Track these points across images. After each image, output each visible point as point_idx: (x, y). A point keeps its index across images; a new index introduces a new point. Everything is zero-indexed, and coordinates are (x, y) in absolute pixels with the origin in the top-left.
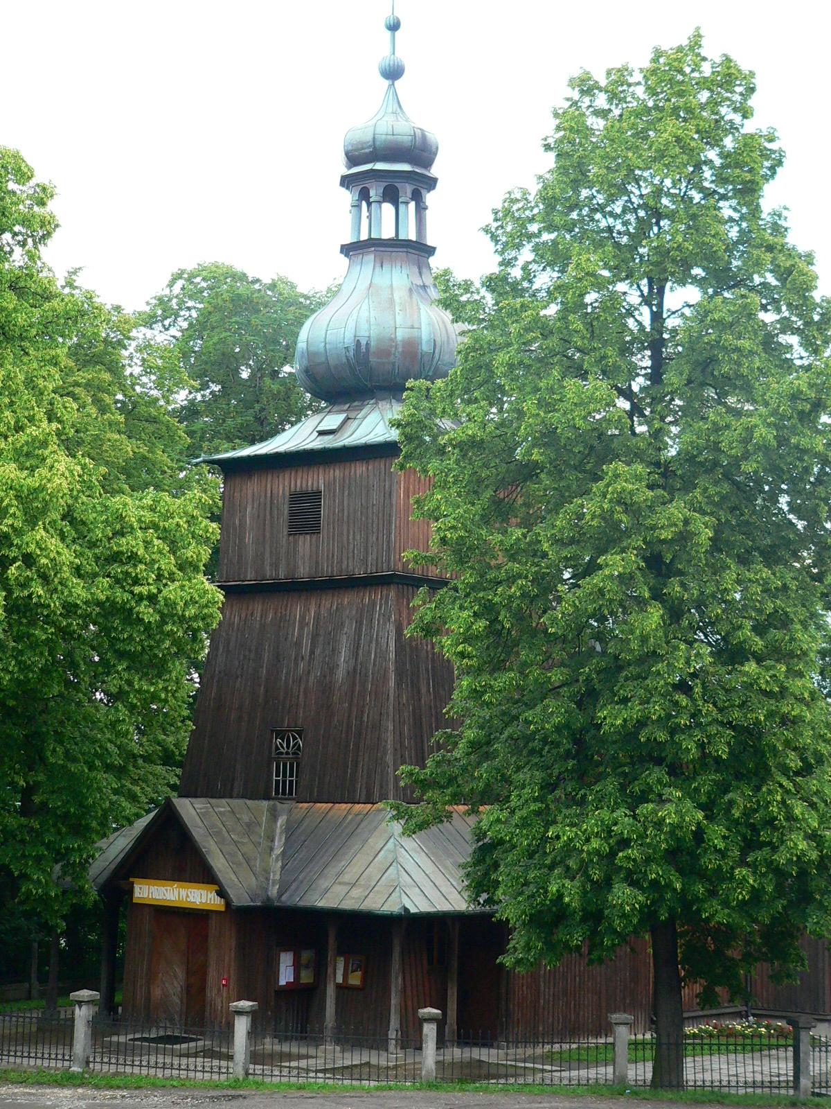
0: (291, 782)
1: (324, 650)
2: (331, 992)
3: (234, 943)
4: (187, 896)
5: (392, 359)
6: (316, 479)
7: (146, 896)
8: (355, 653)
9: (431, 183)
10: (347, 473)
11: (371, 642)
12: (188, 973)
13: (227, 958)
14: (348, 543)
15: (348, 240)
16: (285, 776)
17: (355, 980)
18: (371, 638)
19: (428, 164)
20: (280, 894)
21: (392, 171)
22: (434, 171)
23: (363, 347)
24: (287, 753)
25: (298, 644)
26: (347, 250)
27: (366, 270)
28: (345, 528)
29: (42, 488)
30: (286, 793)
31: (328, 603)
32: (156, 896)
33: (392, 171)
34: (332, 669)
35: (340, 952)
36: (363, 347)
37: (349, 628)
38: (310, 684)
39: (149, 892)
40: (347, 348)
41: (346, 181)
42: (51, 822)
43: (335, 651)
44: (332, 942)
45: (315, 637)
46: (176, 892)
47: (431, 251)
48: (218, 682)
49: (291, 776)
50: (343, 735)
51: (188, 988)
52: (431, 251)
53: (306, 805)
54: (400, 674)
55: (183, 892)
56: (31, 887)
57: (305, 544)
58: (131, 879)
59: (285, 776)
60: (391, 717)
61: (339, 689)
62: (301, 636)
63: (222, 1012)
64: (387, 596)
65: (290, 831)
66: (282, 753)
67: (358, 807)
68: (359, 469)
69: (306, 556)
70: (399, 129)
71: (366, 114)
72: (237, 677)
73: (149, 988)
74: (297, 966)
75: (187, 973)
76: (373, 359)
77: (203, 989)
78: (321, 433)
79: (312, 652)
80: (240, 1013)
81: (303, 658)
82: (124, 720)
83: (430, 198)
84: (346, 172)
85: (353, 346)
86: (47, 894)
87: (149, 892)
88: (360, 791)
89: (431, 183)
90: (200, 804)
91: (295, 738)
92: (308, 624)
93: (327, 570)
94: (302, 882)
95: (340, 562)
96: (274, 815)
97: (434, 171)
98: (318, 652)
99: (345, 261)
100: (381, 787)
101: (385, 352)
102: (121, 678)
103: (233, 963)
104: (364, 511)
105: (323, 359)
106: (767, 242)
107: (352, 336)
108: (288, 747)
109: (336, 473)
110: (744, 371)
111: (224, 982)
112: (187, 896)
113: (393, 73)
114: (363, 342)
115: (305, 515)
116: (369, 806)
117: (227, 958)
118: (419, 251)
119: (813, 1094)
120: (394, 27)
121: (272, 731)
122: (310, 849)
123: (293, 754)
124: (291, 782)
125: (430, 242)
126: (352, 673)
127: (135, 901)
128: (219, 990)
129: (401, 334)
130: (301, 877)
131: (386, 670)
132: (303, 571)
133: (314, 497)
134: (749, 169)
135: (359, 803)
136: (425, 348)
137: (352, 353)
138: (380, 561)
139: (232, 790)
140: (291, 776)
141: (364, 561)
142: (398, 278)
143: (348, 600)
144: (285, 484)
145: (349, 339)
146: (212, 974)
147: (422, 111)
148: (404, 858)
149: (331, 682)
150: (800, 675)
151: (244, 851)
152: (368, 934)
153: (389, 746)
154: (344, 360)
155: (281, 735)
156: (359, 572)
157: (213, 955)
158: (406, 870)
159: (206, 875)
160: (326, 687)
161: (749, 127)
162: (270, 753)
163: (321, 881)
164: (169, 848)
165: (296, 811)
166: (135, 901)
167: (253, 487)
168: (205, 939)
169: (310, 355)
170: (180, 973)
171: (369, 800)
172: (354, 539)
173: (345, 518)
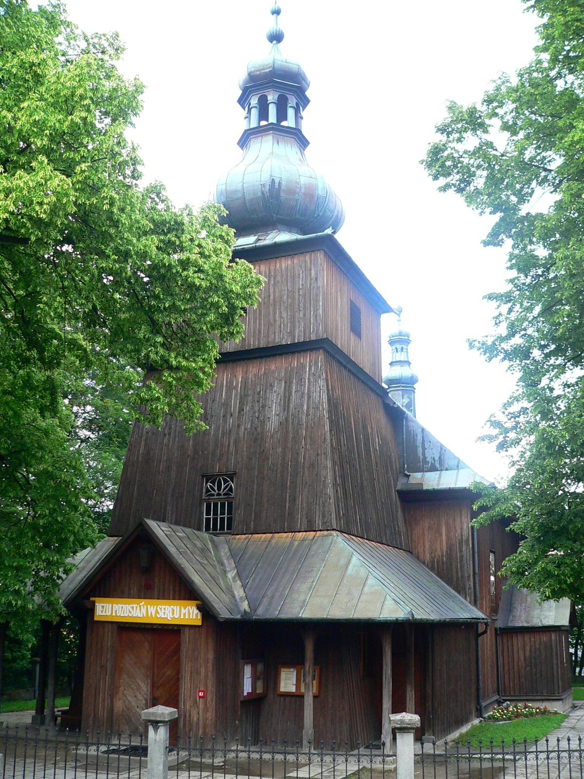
0: (222, 520)
1: (253, 407)
3: (211, 656)
4: (157, 612)
5: (296, 197)
7: (109, 614)
8: (286, 406)
10: (272, 268)
11: (302, 397)
13: (203, 670)
14: (275, 321)
16: (215, 513)
18: (303, 393)
20: (253, 607)
23: (277, 184)
24: (219, 494)
25: (226, 405)
28: (271, 309)
32: (120, 613)
36: (277, 184)
37: (279, 388)
38: (241, 434)
39: (110, 610)
40: (263, 185)
42: (30, 535)
45: (243, 398)
46: (144, 611)
48: (146, 440)
49: (223, 513)
50: (279, 475)
53: (244, 536)
55: (152, 610)
56: (11, 598)
58: (92, 599)
59: (215, 513)
60: (329, 455)
61: (272, 436)
62: (229, 396)
63: (198, 723)
64: (316, 363)
65: (233, 555)
66: (213, 495)
67: (300, 535)
71: (264, 56)
72: (165, 435)
73: (112, 702)
74: (255, 678)
75: (153, 686)
76: (282, 195)
79: (241, 410)
80: (156, 724)
81: (231, 415)
82: (158, 398)
85: (268, 183)
86: (24, 607)
87: (110, 610)
88: (300, 520)
91: (226, 481)
92: (236, 388)
94: (273, 597)
95: (268, 336)
98: (247, 408)
100: (324, 516)
101: (291, 192)
102: (157, 353)
103: (210, 674)
104: (290, 294)
105: (240, 195)
107: (269, 177)
108: (219, 489)
111: (201, 694)
112: (157, 612)
114: (277, 181)
116: (312, 533)
117: (203, 670)
121: (203, 476)
123: (224, 494)
124: (222, 520)
126: (284, 425)
127: (96, 619)
128: (195, 702)
130: (269, 593)
131: (321, 418)
135: (299, 532)
137: (267, 188)
138: (307, 332)
140: (223, 513)
141: (292, 334)
143: (278, 366)
145: (265, 178)
149: (262, 433)
153: (329, 480)
154: (260, 194)
155: (210, 478)
157: (187, 667)
159: (185, 591)
160: (257, 437)
162: (201, 494)
163: (295, 596)
164: (140, 564)
165: (235, 541)
166: (96, 619)
168: (177, 651)
172: (281, 317)
173: (271, 302)
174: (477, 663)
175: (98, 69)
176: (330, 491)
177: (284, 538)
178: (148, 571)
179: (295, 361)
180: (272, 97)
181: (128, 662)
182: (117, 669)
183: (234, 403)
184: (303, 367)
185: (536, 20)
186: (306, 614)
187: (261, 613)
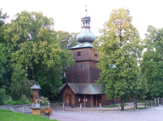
6: (80, 50)
8: (85, 68)
9: (90, 21)
12: (69, 101)
15: (82, 26)
19: (90, 19)
21: (87, 20)
22: (90, 20)
25: (79, 67)
26: (82, 28)
27: (84, 29)
30: (78, 82)
31: (82, 63)
33: (87, 20)
34: (82, 70)
41: (82, 21)
43: (83, 68)
45: (80, 66)
47: (90, 28)
51: (69, 102)
52: (90, 28)
54: (90, 70)
57: (79, 57)
68: (85, 49)
69: (79, 58)
70: (88, 16)
71: (84, 15)
76: (86, 38)
77: (71, 102)
83: (90, 22)
88: (86, 82)
89: (90, 21)
93: (81, 60)
96: (77, 85)
97: (90, 20)
99: (81, 29)
101: (87, 38)
106: (131, 27)
109: (82, 50)
110: (136, 41)
115: (79, 54)
118: (89, 27)
119: (77, 62)
120: (86, 6)
122: (81, 88)
125: (90, 27)
126: (85, 70)
129: (88, 36)
133: (80, 52)
134: (129, 20)
142: (87, 30)
143: (84, 63)
144: (77, 51)
146: (72, 101)
148: (92, 89)
150: (161, 84)
151: (74, 88)
152: (88, 96)
156: (85, 60)
157: (72, 99)
158: (92, 90)
160: (82, 72)
161: (129, 16)
168: (71, 97)
169: (79, 38)
170: (69, 101)
171: (87, 83)
174: (68, 111)
175: (111, 23)
176: (89, 79)
177: (84, 84)
178: (68, 88)
179: (86, 62)
180: (85, 22)
181: (67, 98)
182: (66, 99)
183: (79, 67)
184: (87, 63)
185: (161, 29)
186: (84, 93)
187: (80, 93)
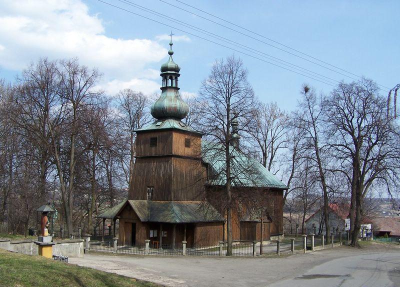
2: (161, 238)
6: (156, 135)
8: (164, 171)
9: (179, 75)
17: (165, 236)
22: (179, 73)
29: (301, 125)
34: (160, 174)
35: (163, 230)
43: (160, 170)
44: (161, 228)
57: (154, 149)
68: (165, 133)
78: (157, 126)
80: (147, 242)
83: (179, 78)
84: (161, 73)
90: (134, 201)
97: (179, 73)
109: (160, 134)
113: (171, 54)
120: (171, 45)
126: (164, 175)
129: (173, 106)
132: (153, 154)
136: (178, 109)
139: (168, 199)
147: (177, 61)
167: (143, 136)
